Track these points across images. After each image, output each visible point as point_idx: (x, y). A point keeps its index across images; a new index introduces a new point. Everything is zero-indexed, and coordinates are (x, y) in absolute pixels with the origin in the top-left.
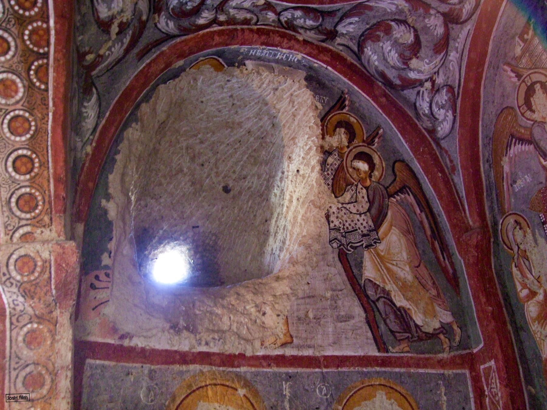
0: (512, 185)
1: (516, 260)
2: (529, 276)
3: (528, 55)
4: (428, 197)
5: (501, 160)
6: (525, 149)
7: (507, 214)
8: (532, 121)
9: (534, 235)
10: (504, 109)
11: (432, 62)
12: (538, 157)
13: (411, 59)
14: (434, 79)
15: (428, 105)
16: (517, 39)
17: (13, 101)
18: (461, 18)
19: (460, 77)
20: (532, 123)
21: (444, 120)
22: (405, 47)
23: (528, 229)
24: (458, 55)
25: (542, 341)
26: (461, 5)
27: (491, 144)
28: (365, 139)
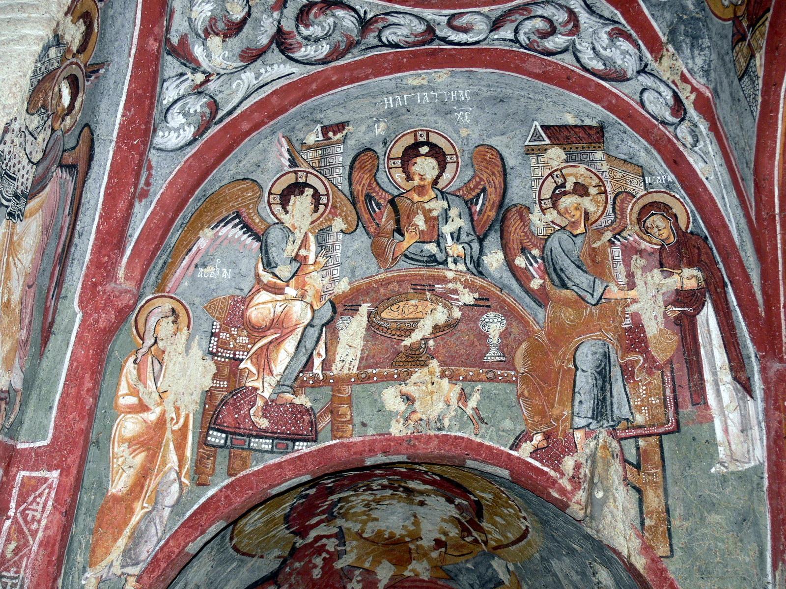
0: (196, 266)
1: (140, 355)
2: (150, 383)
3: (320, 152)
4: (83, 201)
5: (201, 229)
6: (245, 240)
7: (166, 294)
8: (277, 218)
9: (190, 339)
10: (248, 179)
11: (228, 61)
12: (257, 260)
13: (217, 34)
14: (211, 78)
15: (176, 98)
16: (319, 127)
18: (293, 53)
19: (238, 105)
20: (276, 221)
21: (177, 130)
22: (225, 16)
23: (186, 328)
24: (255, 82)
25: (121, 471)
26: (304, 42)
27: (201, 202)
28: (88, 63)
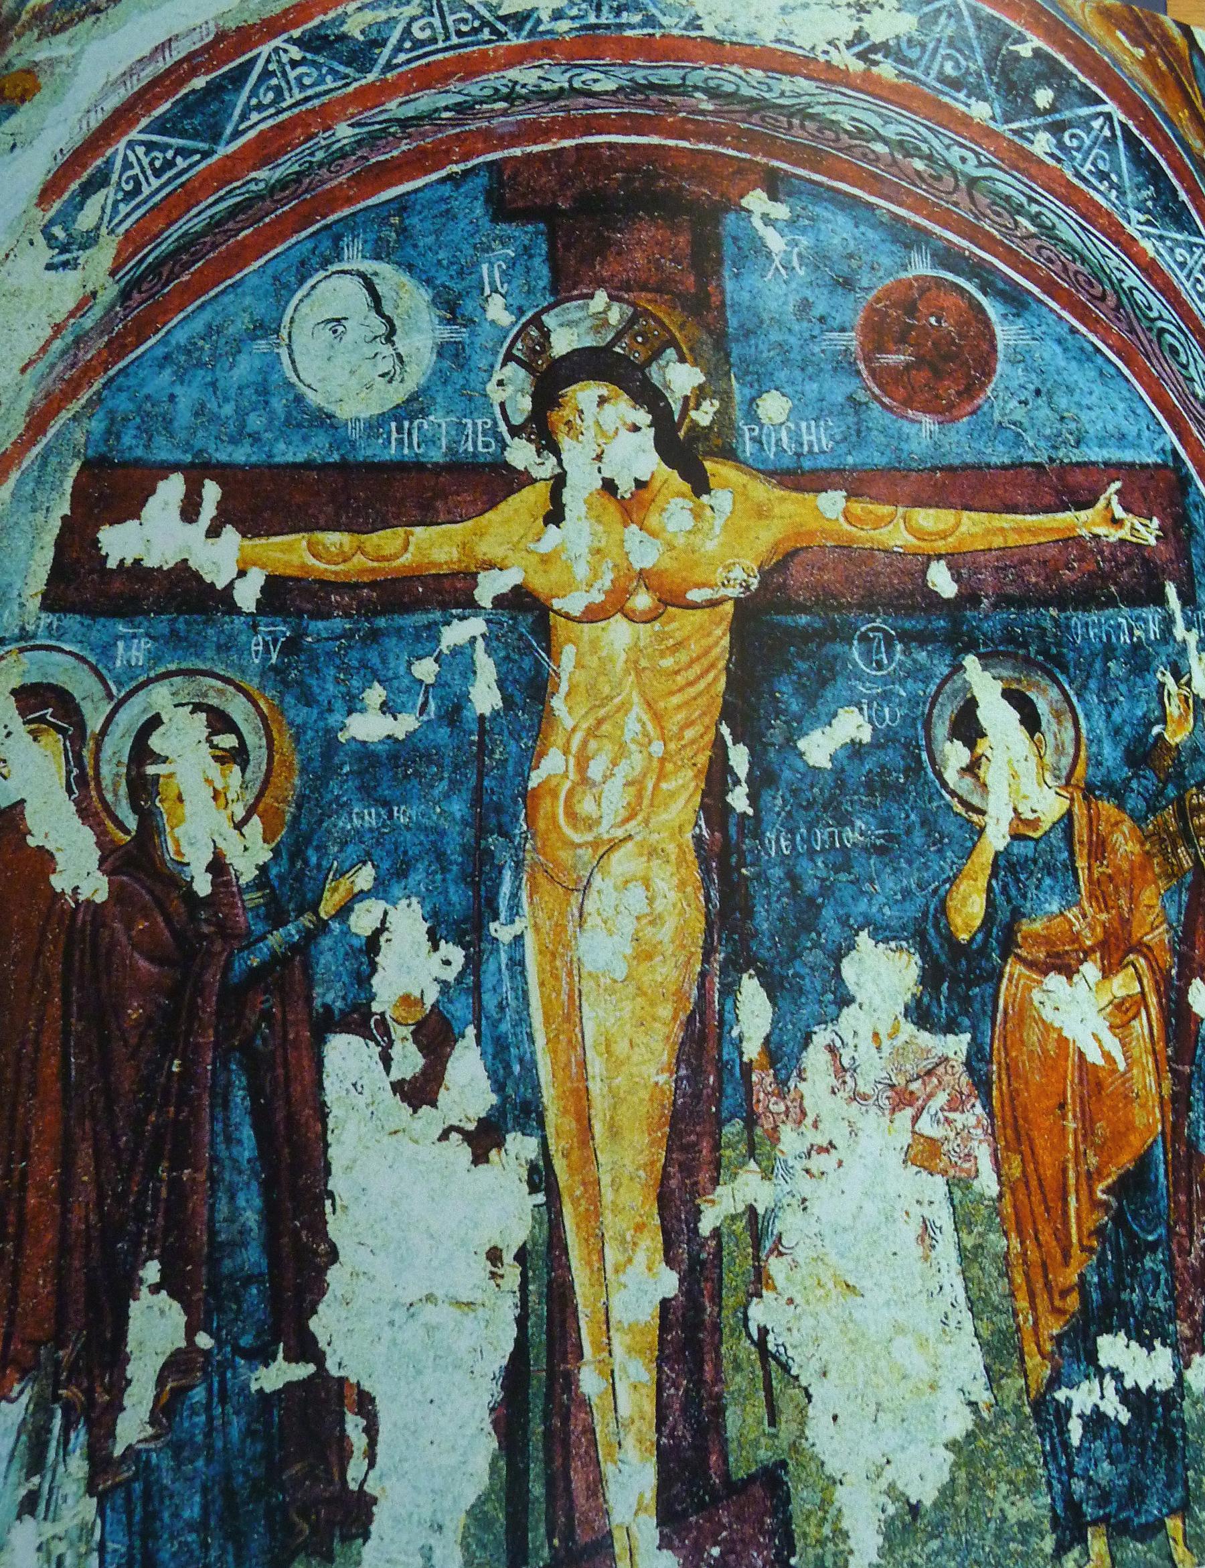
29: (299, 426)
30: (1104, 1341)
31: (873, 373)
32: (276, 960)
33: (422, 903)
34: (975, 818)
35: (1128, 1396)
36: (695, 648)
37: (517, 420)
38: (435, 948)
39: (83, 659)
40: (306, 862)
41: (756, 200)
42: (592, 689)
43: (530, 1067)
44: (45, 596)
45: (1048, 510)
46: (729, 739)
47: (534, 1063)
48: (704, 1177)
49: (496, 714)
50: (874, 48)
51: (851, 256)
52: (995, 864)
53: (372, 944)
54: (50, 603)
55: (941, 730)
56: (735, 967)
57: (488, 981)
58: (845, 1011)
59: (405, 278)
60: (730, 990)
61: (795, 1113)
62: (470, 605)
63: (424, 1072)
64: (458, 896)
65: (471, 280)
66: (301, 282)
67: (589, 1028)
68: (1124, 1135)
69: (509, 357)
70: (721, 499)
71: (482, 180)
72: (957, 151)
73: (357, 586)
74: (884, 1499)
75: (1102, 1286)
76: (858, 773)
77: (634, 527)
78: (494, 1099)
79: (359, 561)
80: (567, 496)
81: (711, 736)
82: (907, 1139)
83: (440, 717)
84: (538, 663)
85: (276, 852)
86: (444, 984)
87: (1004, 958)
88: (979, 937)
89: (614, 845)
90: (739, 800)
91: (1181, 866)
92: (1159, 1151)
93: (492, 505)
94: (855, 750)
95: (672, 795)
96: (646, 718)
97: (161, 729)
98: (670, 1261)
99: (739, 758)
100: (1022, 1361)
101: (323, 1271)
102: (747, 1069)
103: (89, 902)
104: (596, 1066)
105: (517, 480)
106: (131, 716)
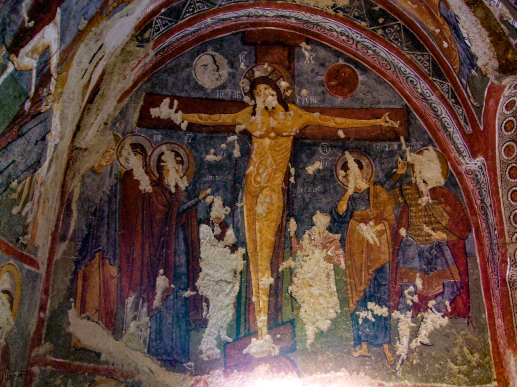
17: (512, 157)
29: (196, 89)
30: (369, 303)
31: (328, 86)
32: (189, 208)
33: (222, 197)
34: (345, 187)
35: (375, 316)
36: (284, 146)
37: (246, 91)
38: (224, 207)
39: (146, 138)
40: (196, 187)
41: (303, 44)
42: (260, 154)
43: (244, 234)
44: (138, 123)
45: (368, 119)
46: (290, 167)
47: (245, 233)
48: (280, 259)
49: (239, 157)
50: (338, 9)
51: (324, 59)
52: (350, 198)
53: (210, 206)
54: (139, 125)
55: (339, 167)
56: (290, 215)
57: (236, 215)
58: (313, 227)
59: (221, 56)
60: (288, 221)
61: (301, 248)
62: (234, 133)
63: (221, 233)
64: (229, 196)
65: (237, 58)
66: (198, 56)
67: (257, 227)
68: (378, 260)
69: (245, 77)
70: (292, 113)
71: (240, 35)
72: (356, 35)
73: (208, 126)
74: (315, 329)
75: (370, 291)
76: (318, 176)
77: (271, 118)
78: (236, 240)
79: (210, 121)
80: (257, 109)
81: (286, 166)
82: (325, 255)
83: (226, 157)
84: (249, 147)
85: (190, 184)
86: (226, 215)
87: (350, 218)
88: (345, 214)
89: (264, 188)
90: (292, 180)
91: (399, 202)
92: (388, 265)
93: (240, 110)
94: (319, 171)
95: (277, 178)
96: (272, 160)
97: (164, 155)
98: (272, 276)
99: (292, 171)
100: (349, 305)
101: (198, 273)
102: (291, 238)
103: (148, 192)
104: (258, 235)
105: (245, 105)
106: (157, 152)
